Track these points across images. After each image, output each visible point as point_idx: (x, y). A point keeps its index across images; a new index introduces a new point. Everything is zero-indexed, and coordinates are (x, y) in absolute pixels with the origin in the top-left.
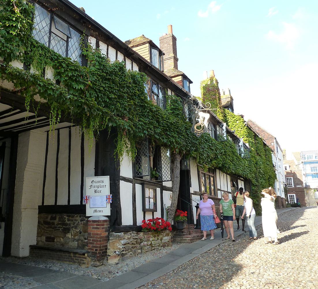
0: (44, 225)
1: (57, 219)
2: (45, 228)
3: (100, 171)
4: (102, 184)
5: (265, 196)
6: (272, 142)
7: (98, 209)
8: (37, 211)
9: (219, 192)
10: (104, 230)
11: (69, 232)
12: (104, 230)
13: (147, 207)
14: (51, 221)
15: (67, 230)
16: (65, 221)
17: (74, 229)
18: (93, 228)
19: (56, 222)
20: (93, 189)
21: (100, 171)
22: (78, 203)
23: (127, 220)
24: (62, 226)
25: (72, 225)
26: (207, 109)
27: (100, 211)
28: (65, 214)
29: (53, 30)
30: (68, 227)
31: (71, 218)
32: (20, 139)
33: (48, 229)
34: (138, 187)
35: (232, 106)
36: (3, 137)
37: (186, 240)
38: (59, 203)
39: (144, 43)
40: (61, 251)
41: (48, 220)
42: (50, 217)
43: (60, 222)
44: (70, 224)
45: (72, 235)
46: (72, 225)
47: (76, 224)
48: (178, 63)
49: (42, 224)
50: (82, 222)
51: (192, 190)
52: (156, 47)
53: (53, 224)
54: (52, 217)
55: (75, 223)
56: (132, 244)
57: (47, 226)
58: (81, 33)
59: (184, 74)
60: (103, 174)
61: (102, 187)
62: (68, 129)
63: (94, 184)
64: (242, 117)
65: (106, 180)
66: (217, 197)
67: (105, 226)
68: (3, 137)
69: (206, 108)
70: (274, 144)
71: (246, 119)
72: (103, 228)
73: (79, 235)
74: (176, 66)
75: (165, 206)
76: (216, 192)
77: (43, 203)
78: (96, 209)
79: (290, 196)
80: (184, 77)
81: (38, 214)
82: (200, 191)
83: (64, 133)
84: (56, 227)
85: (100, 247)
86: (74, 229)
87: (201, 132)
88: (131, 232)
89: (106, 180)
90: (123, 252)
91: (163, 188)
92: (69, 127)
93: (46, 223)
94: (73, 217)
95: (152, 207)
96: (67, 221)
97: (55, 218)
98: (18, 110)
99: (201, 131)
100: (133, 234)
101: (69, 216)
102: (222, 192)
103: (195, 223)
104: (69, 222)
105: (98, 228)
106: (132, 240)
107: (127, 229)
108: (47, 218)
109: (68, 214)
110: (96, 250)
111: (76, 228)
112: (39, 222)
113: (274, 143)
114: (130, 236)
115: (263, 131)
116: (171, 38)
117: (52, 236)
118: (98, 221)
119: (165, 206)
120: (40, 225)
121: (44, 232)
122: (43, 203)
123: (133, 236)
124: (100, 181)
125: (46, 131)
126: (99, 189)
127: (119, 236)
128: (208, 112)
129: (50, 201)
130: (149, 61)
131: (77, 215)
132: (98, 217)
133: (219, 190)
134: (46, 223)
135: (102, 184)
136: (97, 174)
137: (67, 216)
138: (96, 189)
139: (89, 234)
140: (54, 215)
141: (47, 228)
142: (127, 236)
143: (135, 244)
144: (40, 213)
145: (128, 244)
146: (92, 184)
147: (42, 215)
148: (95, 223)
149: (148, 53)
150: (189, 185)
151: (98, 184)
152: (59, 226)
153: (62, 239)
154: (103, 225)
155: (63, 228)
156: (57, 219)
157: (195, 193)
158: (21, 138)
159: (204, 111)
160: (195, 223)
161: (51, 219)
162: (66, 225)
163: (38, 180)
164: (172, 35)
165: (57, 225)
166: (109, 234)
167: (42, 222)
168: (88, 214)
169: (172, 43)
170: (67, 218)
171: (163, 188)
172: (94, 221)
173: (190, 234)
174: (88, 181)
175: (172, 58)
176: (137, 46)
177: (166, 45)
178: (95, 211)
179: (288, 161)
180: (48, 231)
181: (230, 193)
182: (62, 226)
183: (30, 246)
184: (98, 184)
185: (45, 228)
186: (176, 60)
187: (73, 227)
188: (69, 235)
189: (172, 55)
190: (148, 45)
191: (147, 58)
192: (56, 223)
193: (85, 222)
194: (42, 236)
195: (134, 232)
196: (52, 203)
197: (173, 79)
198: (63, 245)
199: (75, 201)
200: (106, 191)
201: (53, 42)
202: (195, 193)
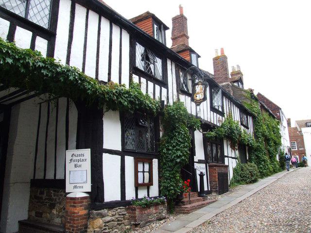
1: (45, 194)
4: (82, 158)
5: (177, 13)
7: (78, 185)
9: (226, 159)
10: (83, 208)
12: (83, 208)
13: (140, 181)
14: (40, 196)
15: (52, 206)
16: (51, 196)
18: (71, 206)
19: (44, 196)
20: (73, 164)
23: (111, 193)
31: (56, 193)
37: (184, 210)
38: (57, 178)
40: (43, 229)
44: (56, 200)
46: (58, 201)
47: (61, 199)
51: (196, 159)
53: (41, 198)
56: (118, 221)
57: (37, 201)
61: (83, 160)
63: (74, 158)
65: (87, 153)
72: (81, 206)
77: (45, 177)
78: (76, 185)
85: (77, 227)
88: (118, 208)
89: (87, 153)
90: (105, 231)
93: (36, 197)
94: (58, 192)
95: (147, 181)
97: (42, 193)
100: (119, 210)
102: (230, 159)
103: (199, 191)
105: (75, 207)
106: (117, 216)
107: (112, 205)
110: (73, 230)
111: (60, 203)
112: (31, 196)
117: (41, 211)
120: (32, 199)
122: (45, 177)
126: (80, 163)
127: (100, 213)
129: (40, 176)
134: (36, 197)
135: (82, 158)
136: (78, 147)
138: (76, 163)
139: (67, 212)
140: (42, 190)
142: (111, 213)
143: (122, 221)
144: (31, 187)
145: (113, 221)
151: (78, 158)
152: (46, 201)
153: (48, 214)
154: (82, 202)
156: (45, 194)
157: (200, 162)
160: (199, 191)
162: (52, 200)
163: (30, 153)
172: (72, 199)
178: (75, 187)
183: (20, 222)
184: (78, 158)
188: (54, 212)
192: (44, 198)
195: (121, 207)
196: (42, 177)
198: (49, 221)
200: (87, 165)
202: (200, 162)
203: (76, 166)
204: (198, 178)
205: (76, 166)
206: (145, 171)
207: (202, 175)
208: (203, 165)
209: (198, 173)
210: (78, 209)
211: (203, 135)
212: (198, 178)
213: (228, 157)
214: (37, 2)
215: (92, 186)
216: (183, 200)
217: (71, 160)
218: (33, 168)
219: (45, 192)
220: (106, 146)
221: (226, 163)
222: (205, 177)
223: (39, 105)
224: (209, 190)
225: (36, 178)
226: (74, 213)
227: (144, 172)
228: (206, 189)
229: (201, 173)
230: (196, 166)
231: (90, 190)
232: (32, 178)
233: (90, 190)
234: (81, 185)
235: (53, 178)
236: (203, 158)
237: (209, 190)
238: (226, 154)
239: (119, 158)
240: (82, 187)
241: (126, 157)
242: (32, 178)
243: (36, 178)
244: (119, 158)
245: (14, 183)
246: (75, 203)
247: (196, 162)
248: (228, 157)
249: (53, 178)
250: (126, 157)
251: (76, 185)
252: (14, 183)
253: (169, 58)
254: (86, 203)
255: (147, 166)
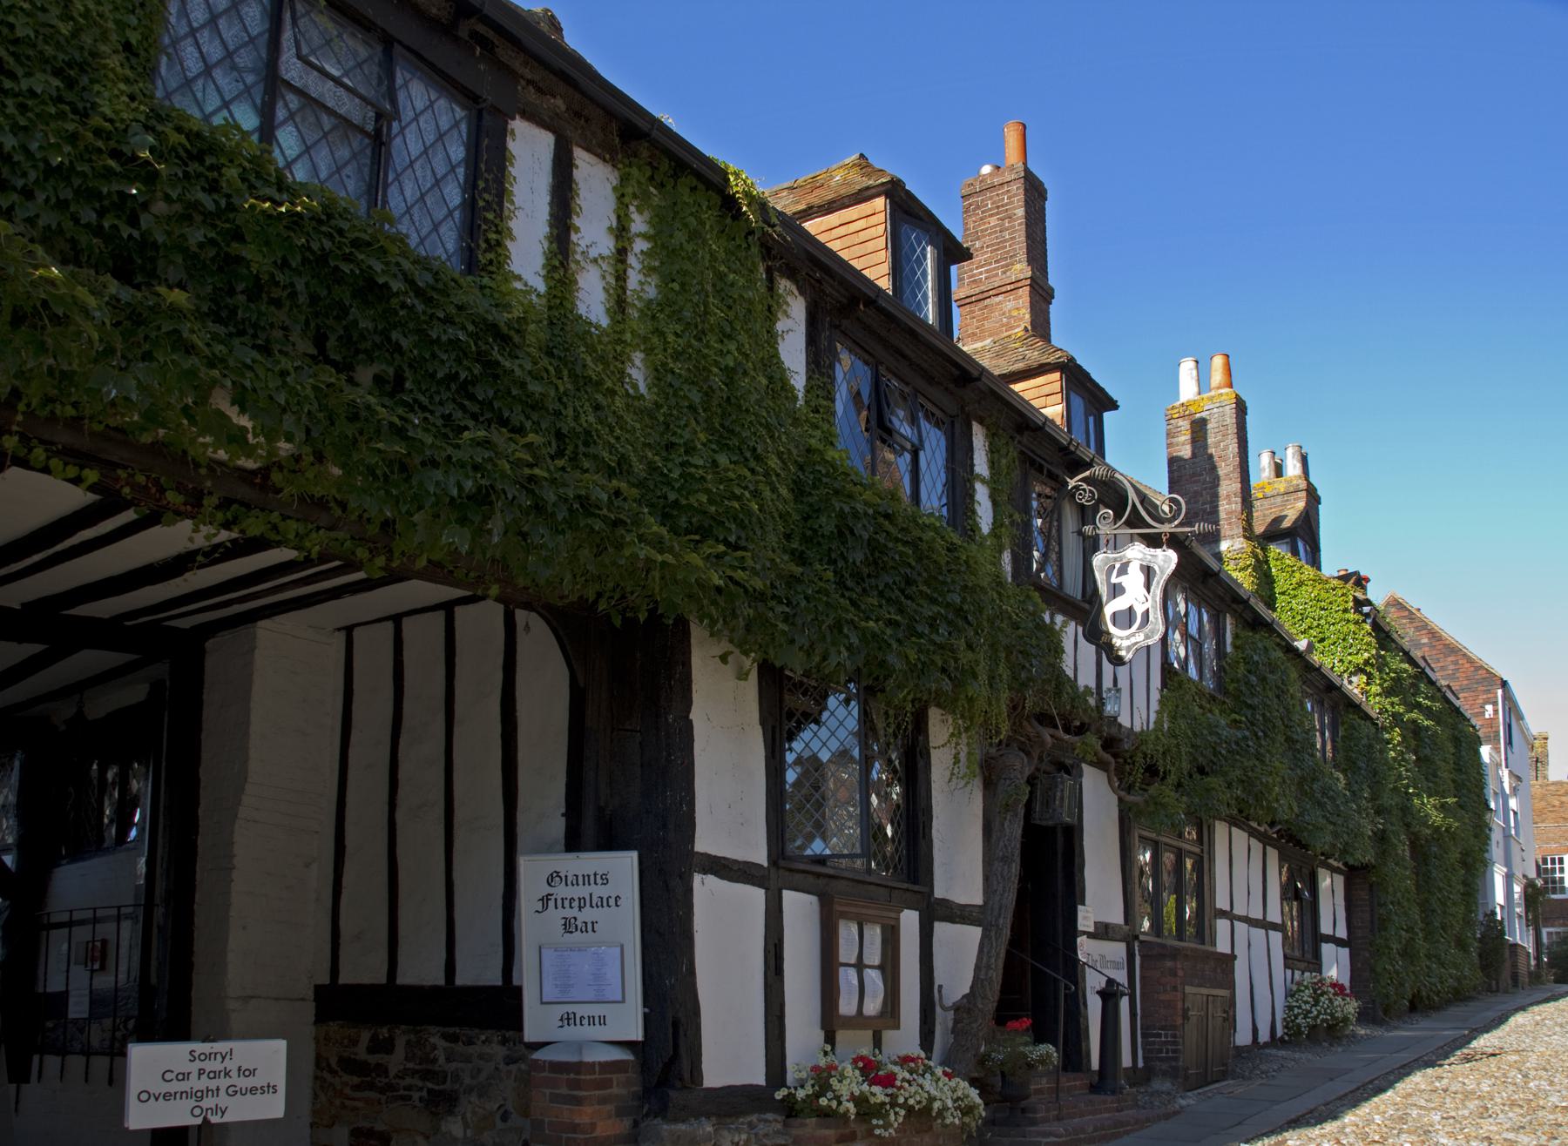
0: (341, 1073)
2: (347, 1091)
3: (589, 826)
4: (599, 891)
6: (1487, 702)
7: (581, 1010)
8: (309, 1010)
9: (1222, 926)
10: (610, 1107)
11: (451, 1112)
12: (610, 1107)
13: (847, 1006)
14: (373, 1059)
15: (443, 1101)
16: (435, 1061)
17: (474, 1098)
18: (555, 1098)
19: (396, 1061)
20: (555, 916)
21: (589, 826)
22: (494, 977)
24: (420, 1084)
25: (467, 1081)
26: (1166, 528)
27: (592, 1020)
28: (433, 1029)
29: (291, 68)
30: (448, 1086)
31: (459, 1048)
32: (210, 663)
33: (358, 1095)
34: (799, 907)
35: (1310, 527)
36: (136, 657)
38: (406, 977)
39: (861, 197)
41: (361, 1052)
42: (365, 1036)
43: (410, 1065)
45: (466, 1126)
48: (1054, 309)
49: (333, 1072)
50: (513, 1067)
51: (1086, 919)
52: (922, 214)
53: (382, 1070)
54: (374, 1038)
55: (479, 1071)
57: (356, 1080)
58: (467, 96)
59: (1072, 360)
60: (609, 842)
61: (603, 903)
62: (440, 616)
63: (561, 891)
64: (1360, 581)
65: (623, 867)
66: (1211, 949)
67: (615, 1090)
68: (136, 657)
69: (1161, 521)
70: (1202, 851)
71: (1377, 594)
72: (603, 1101)
73: (499, 1124)
74: (1040, 327)
75: (940, 991)
76: (1207, 923)
77: (335, 971)
78: (570, 1008)
79: (1549, 934)
80: (1077, 380)
81: (316, 1022)
82: (1127, 921)
83: (424, 636)
84: (390, 1087)
86: (474, 1098)
87: (1133, 640)
89: (623, 867)
91: (935, 911)
92: (448, 607)
95: (873, 1006)
96: (442, 1060)
97: (387, 1047)
98: (129, 516)
99: (1133, 635)
101: (453, 1039)
102: (1241, 927)
104: (453, 1065)
105: (578, 1101)
108: (354, 1042)
109: (447, 1029)
112: (320, 1061)
113: (1495, 704)
114: (744, 1137)
115: (1453, 649)
116: (1017, 189)
117: (379, 1127)
118: (578, 1067)
119: (940, 991)
120: (326, 1075)
121: (343, 1106)
122: (335, 971)
123: (766, 1135)
124: (592, 878)
125: (339, 629)
126: (587, 915)
128: (1175, 542)
129: (364, 968)
130: (885, 284)
131: (489, 1032)
132: (580, 1046)
133: (1223, 914)
135: (599, 891)
136: (573, 843)
137: (445, 1037)
138: (569, 913)
140: (384, 1032)
141: (357, 1088)
144: (321, 1017)
146: (551, 890)
147: (333, 1027)
148: (565, 1076)
149: (881, 242)
150: (1074, 894)
151: (582, 891)
152: (408, 1081)
154: (606, 1084)
155: (424, 1093)
157: (1103, 932)
158: (217, 652)
159: (1153, 541)
161: (371, 1050)
163: (307, 866)
164: (1027, 170)
165: (397, 1076)
166: (636, 1124)
167: (333, 1062)
168: (530, 1034)
169: (1021, 212)
170: (441, 1043)
171: (935, 911)
173: (1058, 1118)
174: (532, 871)
175: (1020, 284)
176: (829, 208)
177: (993, 221)
178: (568, 1019)
179: (1553, 784)
180: (359, 1104)
181: (1274, 927)
182: (420, 1084)
184: (582, 891)
185: (347, 1091)
186: (1041, 295)
187: (470, 1090)
189: (1021, 270)
190: (880, 203)
191: (878, 272)
192: (393, 1071)
193: (523, 1067)
194: (333, 1125)
195: (770, 1116)
196: (432, 975)
197: (1017, 387)
199: (479, 969)
201: (288, 140)
202: (1103, 932)
203: (568, 926)
204: (1094, 1006)
205: (568, 926)
206: (866, 961)
207: (1109, 995)
208: (1117, 950)
209: (1094, 982)
210: (588, 1110)
211: (1120, 800)
212: (1094, 1006)
213: (1228, 915)
214: (199, 16)
215: (646, 1017)
216: (1023, 1104)
217: (545, 900)
218: (327, 936)
219: (400, 1044)
220: (705, 842)
221: (1223, 946)
222: (1124, 1003)
223: (342, 636)
224: (1140, 1064)
225: (344, 979)
226: (575, 1128)
227: (860, 966)
228: (1126, 1061)
229: (1110, 982)
230: (1086, 948)
231: (636, 1033)
232: (325, 979)
233: (636, 1033)
234: (596, 1010)
235: (441, 982)
236: (1116, 917)
237: (1140, 1064)
238: (1222, 903)
239: (757, 896)
240: (603, 1021)
241: (788, 896)
242: (325, 979)
243: (344, 979)
244: (756, 896)
245: (247, 999)
246: (576, 1085)
247: (1084, 933)
248: (1228, 915)
249: (441, 982)
250: (788, 896)
251: (570, 1008)
252: (247, 999)
253: (981, 422)
254: (623, 1091)
255: (874, 934)
